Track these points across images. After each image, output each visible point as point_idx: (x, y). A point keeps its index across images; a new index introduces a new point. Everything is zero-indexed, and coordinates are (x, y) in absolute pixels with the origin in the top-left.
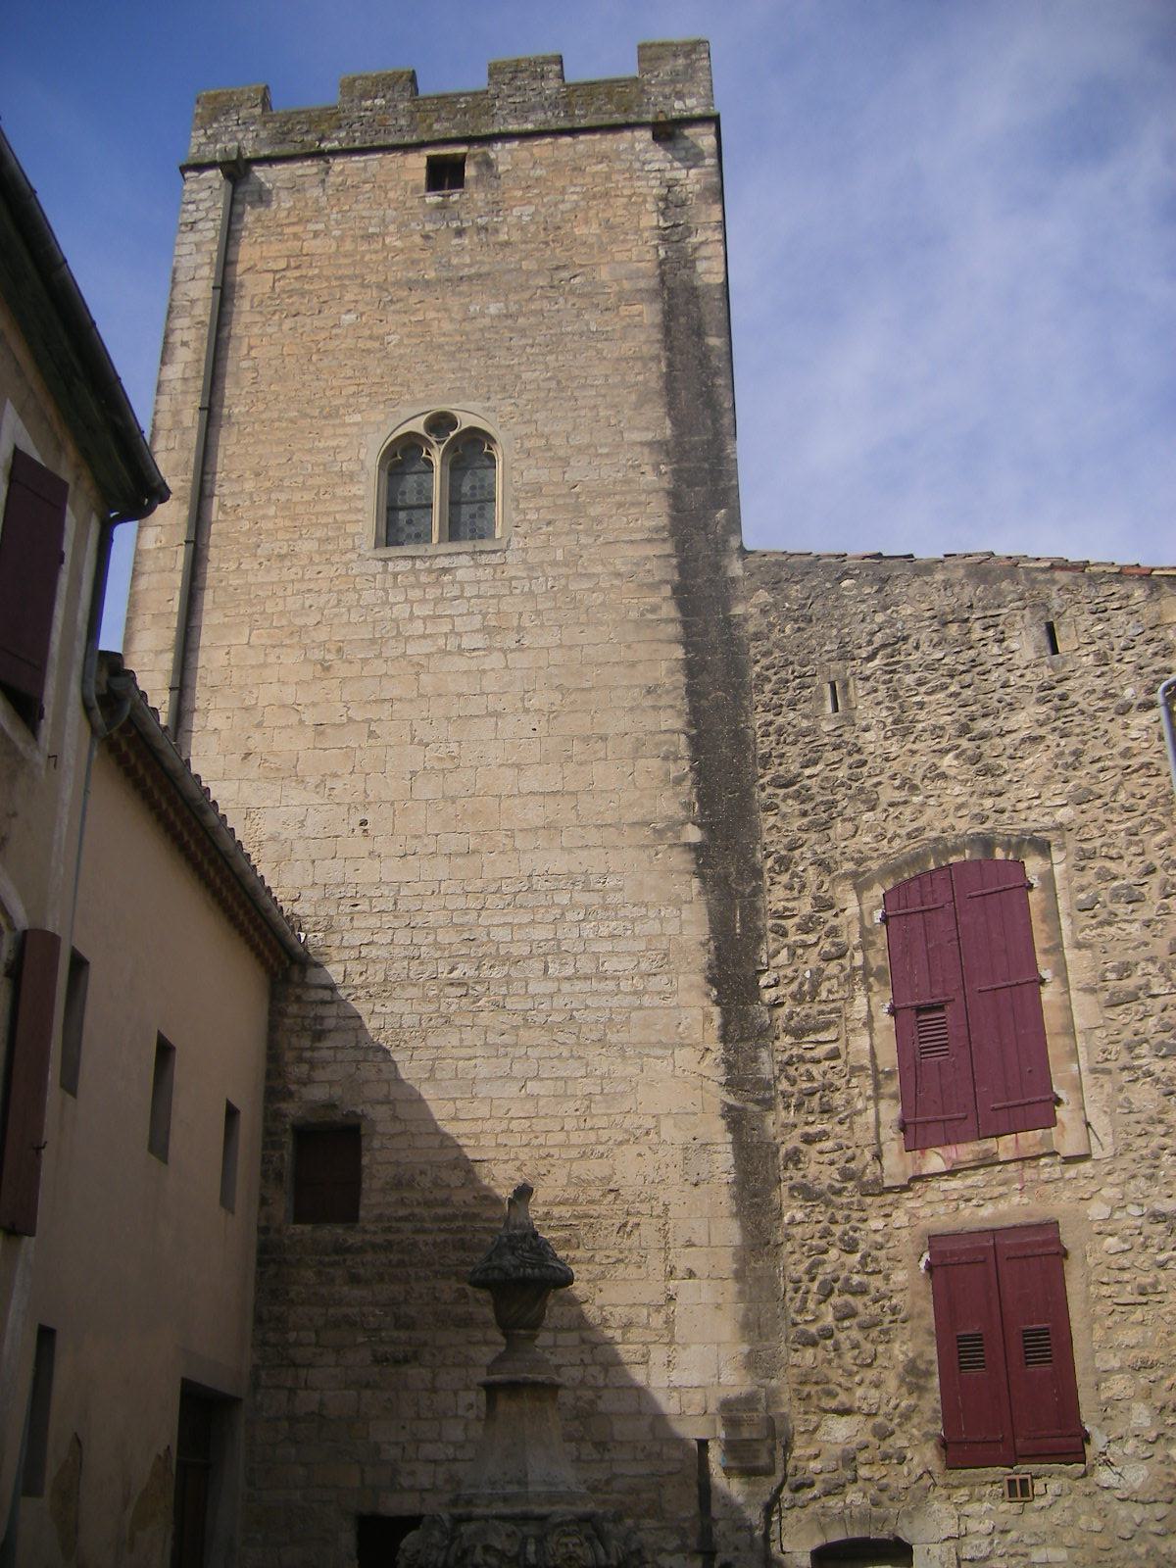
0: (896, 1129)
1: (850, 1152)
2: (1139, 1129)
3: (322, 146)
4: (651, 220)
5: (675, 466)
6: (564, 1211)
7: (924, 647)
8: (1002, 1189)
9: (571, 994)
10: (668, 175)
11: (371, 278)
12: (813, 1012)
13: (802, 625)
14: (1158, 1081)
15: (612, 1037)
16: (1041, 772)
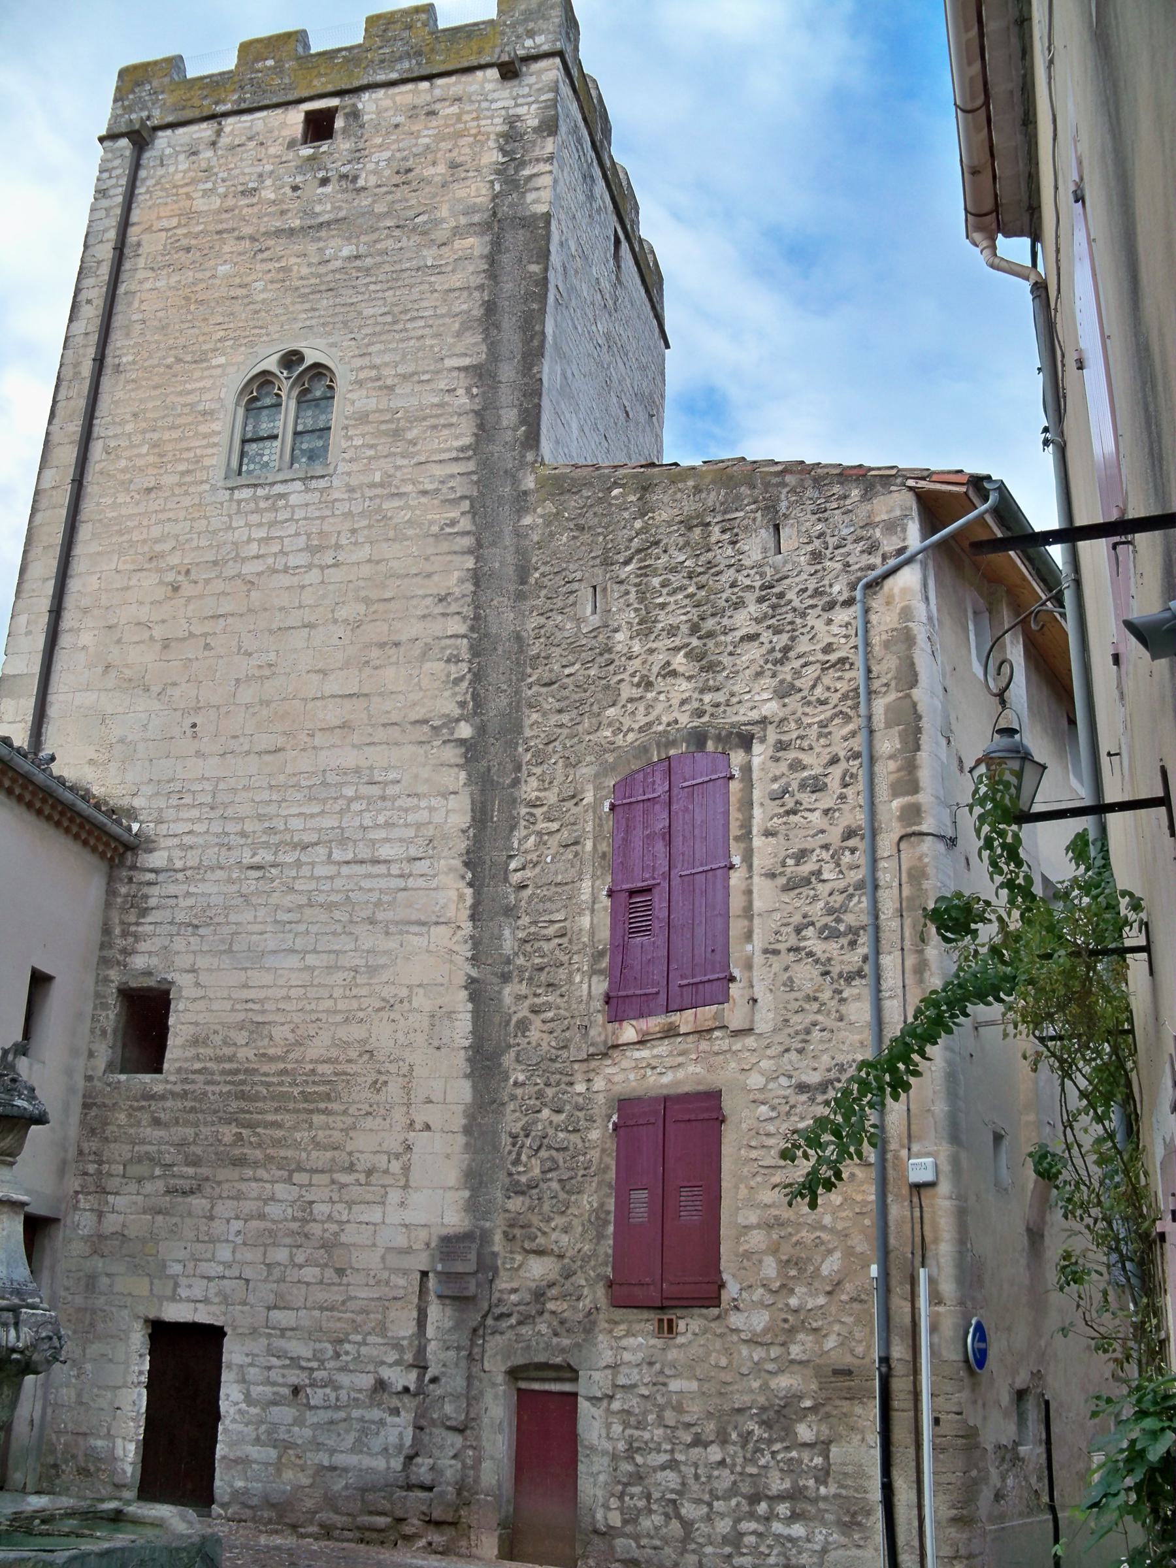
2: (796, 1005)
6: (326, 1069)
7: (671, 551)
8: (681, 1059)
9: (348, 877)
10: (511, 112)
11: (247, 230)
14: (817, 961)
15: (380, 916)
16: (755, 668)
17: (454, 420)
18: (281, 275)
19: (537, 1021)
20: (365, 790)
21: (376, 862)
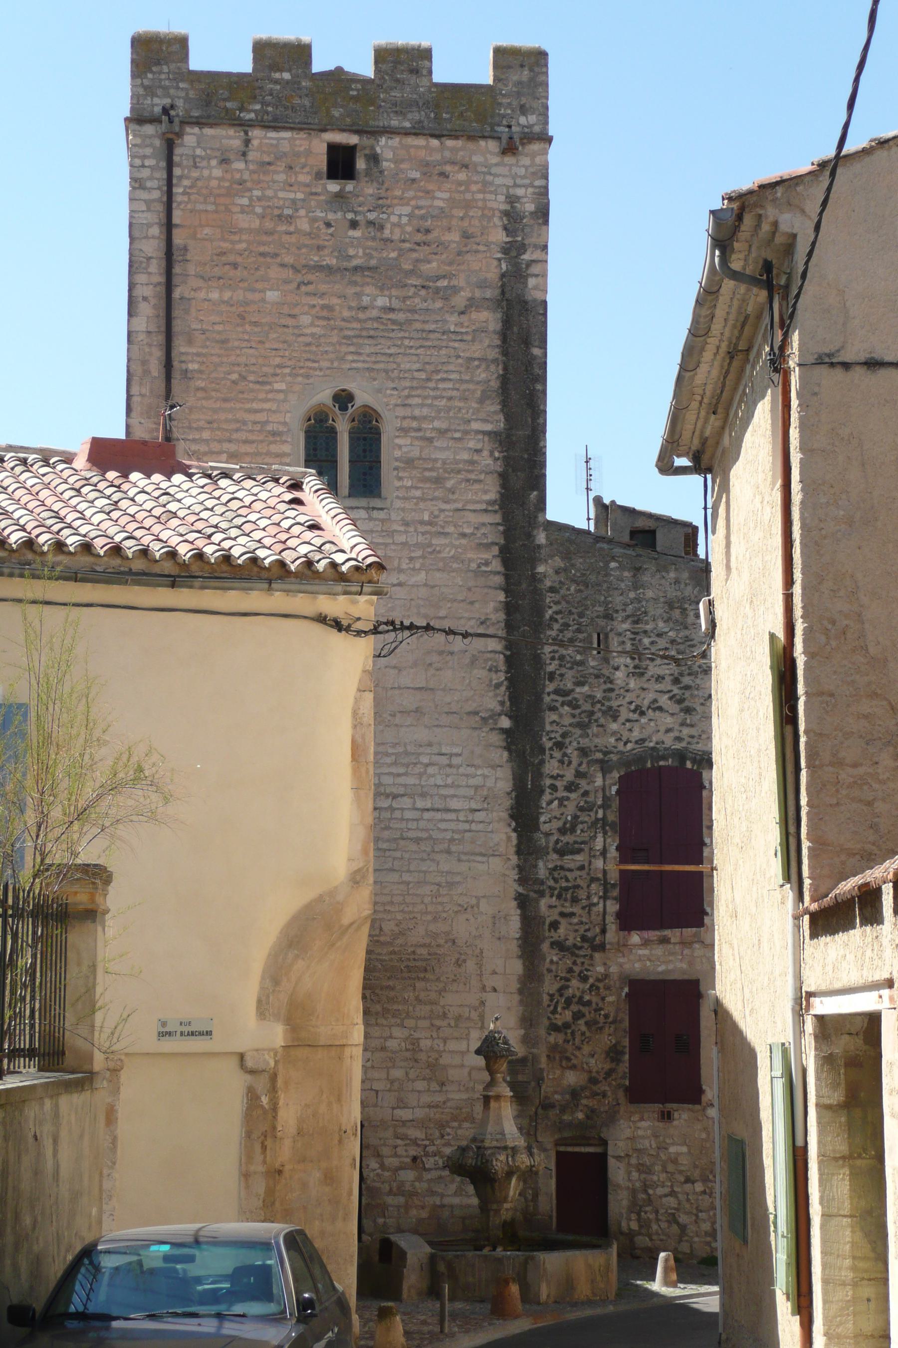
0: (614, 916)
1: (587, 927)
3: (242, 115)
4: (499, 236)
5: (505, 454)
6: (423, 951)
11: (289, 259)
12: (571, 841)
13: (582, 588)
15: (454, 848)
17: (482, 477)
18: (325, 313)
19: (563, 922)
20: (436, 758)
21: (448, 810)
